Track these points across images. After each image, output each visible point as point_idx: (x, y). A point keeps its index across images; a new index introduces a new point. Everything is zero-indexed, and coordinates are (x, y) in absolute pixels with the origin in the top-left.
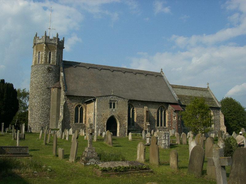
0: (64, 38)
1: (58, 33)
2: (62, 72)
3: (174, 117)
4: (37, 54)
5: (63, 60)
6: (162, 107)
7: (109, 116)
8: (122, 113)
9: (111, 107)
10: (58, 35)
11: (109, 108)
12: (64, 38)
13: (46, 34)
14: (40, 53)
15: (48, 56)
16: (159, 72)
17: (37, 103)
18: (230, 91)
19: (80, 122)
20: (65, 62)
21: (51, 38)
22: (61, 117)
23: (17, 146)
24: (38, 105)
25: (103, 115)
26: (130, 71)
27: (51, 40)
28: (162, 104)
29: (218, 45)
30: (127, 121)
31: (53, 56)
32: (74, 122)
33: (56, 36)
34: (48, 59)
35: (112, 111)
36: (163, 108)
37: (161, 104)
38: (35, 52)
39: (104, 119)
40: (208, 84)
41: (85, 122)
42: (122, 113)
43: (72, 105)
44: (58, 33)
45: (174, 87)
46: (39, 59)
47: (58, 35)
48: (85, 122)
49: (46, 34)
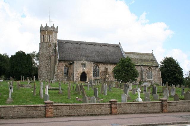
1: (120, 42)
4: (43, 37)
5: (58, 39)
7: (82, 72)
9: (83, 67)
10: (54, 25)
13: (47, 24)
14: (44, 36)
15: (49, 38)
18: (183, 74)
20: (59, 40)
21: (50, 27)
26: (91, 44)
27: (50, 28)
29: (176, 116)
30: (92, 75)
34: (49, 40)
35: (83, 69)
40: (152, 51)
41: (70, 75)
45: (126, 53)
46: (43, 39)
47: (54, 25)
48: (70, 75)
49: (47, 24)
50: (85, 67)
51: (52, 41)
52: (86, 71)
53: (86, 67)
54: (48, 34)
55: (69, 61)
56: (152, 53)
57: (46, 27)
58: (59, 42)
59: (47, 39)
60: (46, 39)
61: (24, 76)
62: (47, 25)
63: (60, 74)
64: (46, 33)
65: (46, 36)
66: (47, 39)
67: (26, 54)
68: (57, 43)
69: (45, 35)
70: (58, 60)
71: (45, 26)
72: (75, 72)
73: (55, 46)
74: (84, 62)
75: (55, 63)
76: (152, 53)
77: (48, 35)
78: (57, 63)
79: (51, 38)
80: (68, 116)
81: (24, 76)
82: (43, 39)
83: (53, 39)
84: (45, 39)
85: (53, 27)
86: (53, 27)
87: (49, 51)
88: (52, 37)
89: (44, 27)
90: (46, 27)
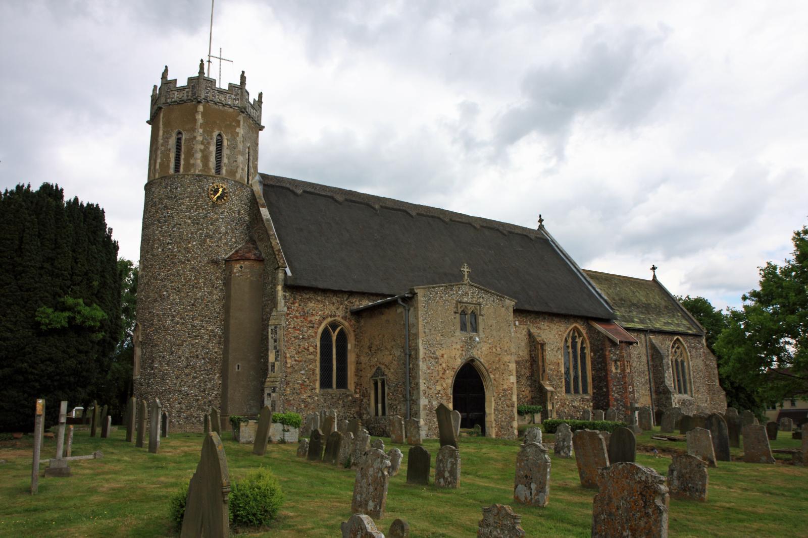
0: (260, 95)
1: (243, 72)
2: (263, 206)
3: (615, 361)
6: (574, 333)
7: (459, 363)
8: (498, 349)
9: (463, 328)
10: (243, 78)
11: (458, 333)
12: (260, 95)
15: (213, 148)
16: (535, 226)
17: (173, 316)
19: (338, 386)
20: (263, 176)
22: (273, 366)
23: (352, 493)
24: (178, 323)
25: (442, 356)
27: (221, 92)
28: (576, 322)
31: (229, 147)
32: (318, 385)
33: (237, 82)
36: (576, 334)
37: (573, 323)
38: (161, 133)
39: (443, 374)
40: (654, 268)
42: (498, 349)
43: (311, 321)
44: (243, 72)
47: (243, 78)
50: (475, 329)
51: (232, 173)
52: (482, 353)
53: (481, 328)
54: (208, 126)
55: (351, 294)
56: (654, 276)
57: (200, 82)
58: (265, 185)
59: (205, 159)
60: (199, 155)
61: (40, 402)
62: (201, 71)
63: (299, 378)
64: (199, 117)
65: (200, 138)
66: (205, 159)
67: (82, 205)
68: (258, 189)
69: (193, 130)
70: (288, 287)
71: (190, 80)
72: (422, 366)
73: (253, 204)
74: (468, 294)
75: (266, 303)
76: (654, 276)
77: (208, 132)
78: (282, 306)
79: (226, 152)
80: (33, 458)
81: (40, 402)
82: (172, 156)
83: (240, 159)
84: (190, 154)
85: (240, 89)
86: (240, 89)
87: (217, 230)
88: (233, 147)
89: (182, 82)
90: (200, 82)
